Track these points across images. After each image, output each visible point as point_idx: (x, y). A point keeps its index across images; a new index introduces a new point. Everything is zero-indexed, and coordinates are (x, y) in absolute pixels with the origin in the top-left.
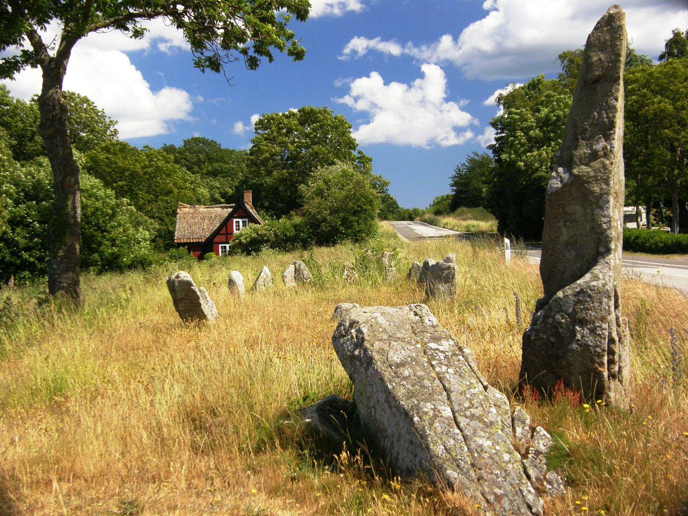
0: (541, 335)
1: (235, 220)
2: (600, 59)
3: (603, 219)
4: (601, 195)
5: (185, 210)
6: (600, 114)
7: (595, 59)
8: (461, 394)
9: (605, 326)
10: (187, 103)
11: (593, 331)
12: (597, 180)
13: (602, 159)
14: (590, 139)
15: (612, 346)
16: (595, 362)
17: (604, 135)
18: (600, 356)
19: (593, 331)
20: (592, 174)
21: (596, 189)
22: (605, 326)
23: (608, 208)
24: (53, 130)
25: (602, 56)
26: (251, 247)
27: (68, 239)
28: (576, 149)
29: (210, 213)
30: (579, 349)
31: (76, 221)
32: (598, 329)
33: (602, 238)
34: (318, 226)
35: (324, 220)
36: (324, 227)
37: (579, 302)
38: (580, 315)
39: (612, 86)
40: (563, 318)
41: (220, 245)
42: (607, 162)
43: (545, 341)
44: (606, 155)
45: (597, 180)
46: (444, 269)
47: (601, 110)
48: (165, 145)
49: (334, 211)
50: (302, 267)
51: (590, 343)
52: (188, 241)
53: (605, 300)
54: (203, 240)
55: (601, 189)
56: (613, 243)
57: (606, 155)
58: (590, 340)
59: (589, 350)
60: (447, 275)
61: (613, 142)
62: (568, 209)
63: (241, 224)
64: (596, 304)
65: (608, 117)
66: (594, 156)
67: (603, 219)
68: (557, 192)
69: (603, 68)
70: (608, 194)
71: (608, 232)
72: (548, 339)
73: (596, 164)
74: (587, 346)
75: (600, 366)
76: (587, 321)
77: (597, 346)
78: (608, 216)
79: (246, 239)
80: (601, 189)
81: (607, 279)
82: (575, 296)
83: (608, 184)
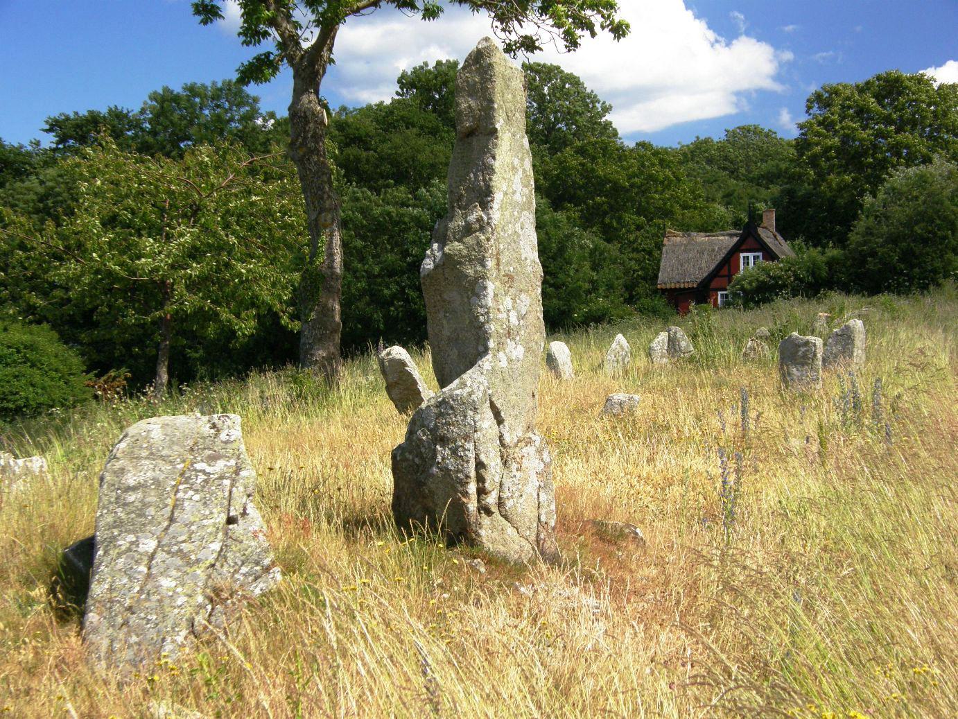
0: (407, 455)
1: (742, 255)
2: (470, 107)
3: (479, 310)
4: (476, 279)
5: (675, 240)
6: (476, 176)
7: (464, 106)
8: (186, 525)
9: (470, 446)
10: (771, 61)
11: (454, 452)
12: (470, 261)
13: (478, 234)
14: (466, 208)
15: (482, 471)
16: (458, 491)
17: (480, 203)
18: (464, 484)
19: (454, 452)
20: (465, 252)
21: (470, 272)
22: (470, 446)
23: (485, 296)
24: (304, 149)
25: (472, 103)
26: (759, 294)
27: (322, 297)
28: (451, 221)
29: (711, 243)
30: (440, 474)
31: (333, 273)
32: (460, 449)
33: (481, 333)
34: (863, 262)
35: (873, 254)
36: (872, 265)
37: (441, 415)
38: (441, 432)
39: (488, 141)
40: (424, 434)
41: (720, 293)
42: (483, 237)
43: (411, 463)
44: (482, 229)
45: (470, 261)
46: (798, 346)
47: (478, 171)
48: (698, 138)
49: (894, 240)
50: (678, 335)
51: (450, 467)
52: (678, 286)
53: (470, 413)
54: (695, 286)
55: (476, 272)
56: (491, 341)
57: (482, 229)
58: (451, 464)
59: (450, 475)
60: (805, 356)
61: (490, 211)
62: (445, 296)
63: (751, 261)
64: (460, 418)
65: (484, 180)
66: (468, 230)
67: (479, 310)
68: (430, 275)
69: (474, 117)
70: (484, 278)
71: (487, 326)
72: (413, 460)
73: (469, 240)
74: (449, 470)
75: (464, 496)
76: (448, 439)
77: (458, 471)
78: (485, 306)
79: (750, 283)
80: (476, 272)
81: (475, 387)
82: (437, 407)
83: (484, 266)
